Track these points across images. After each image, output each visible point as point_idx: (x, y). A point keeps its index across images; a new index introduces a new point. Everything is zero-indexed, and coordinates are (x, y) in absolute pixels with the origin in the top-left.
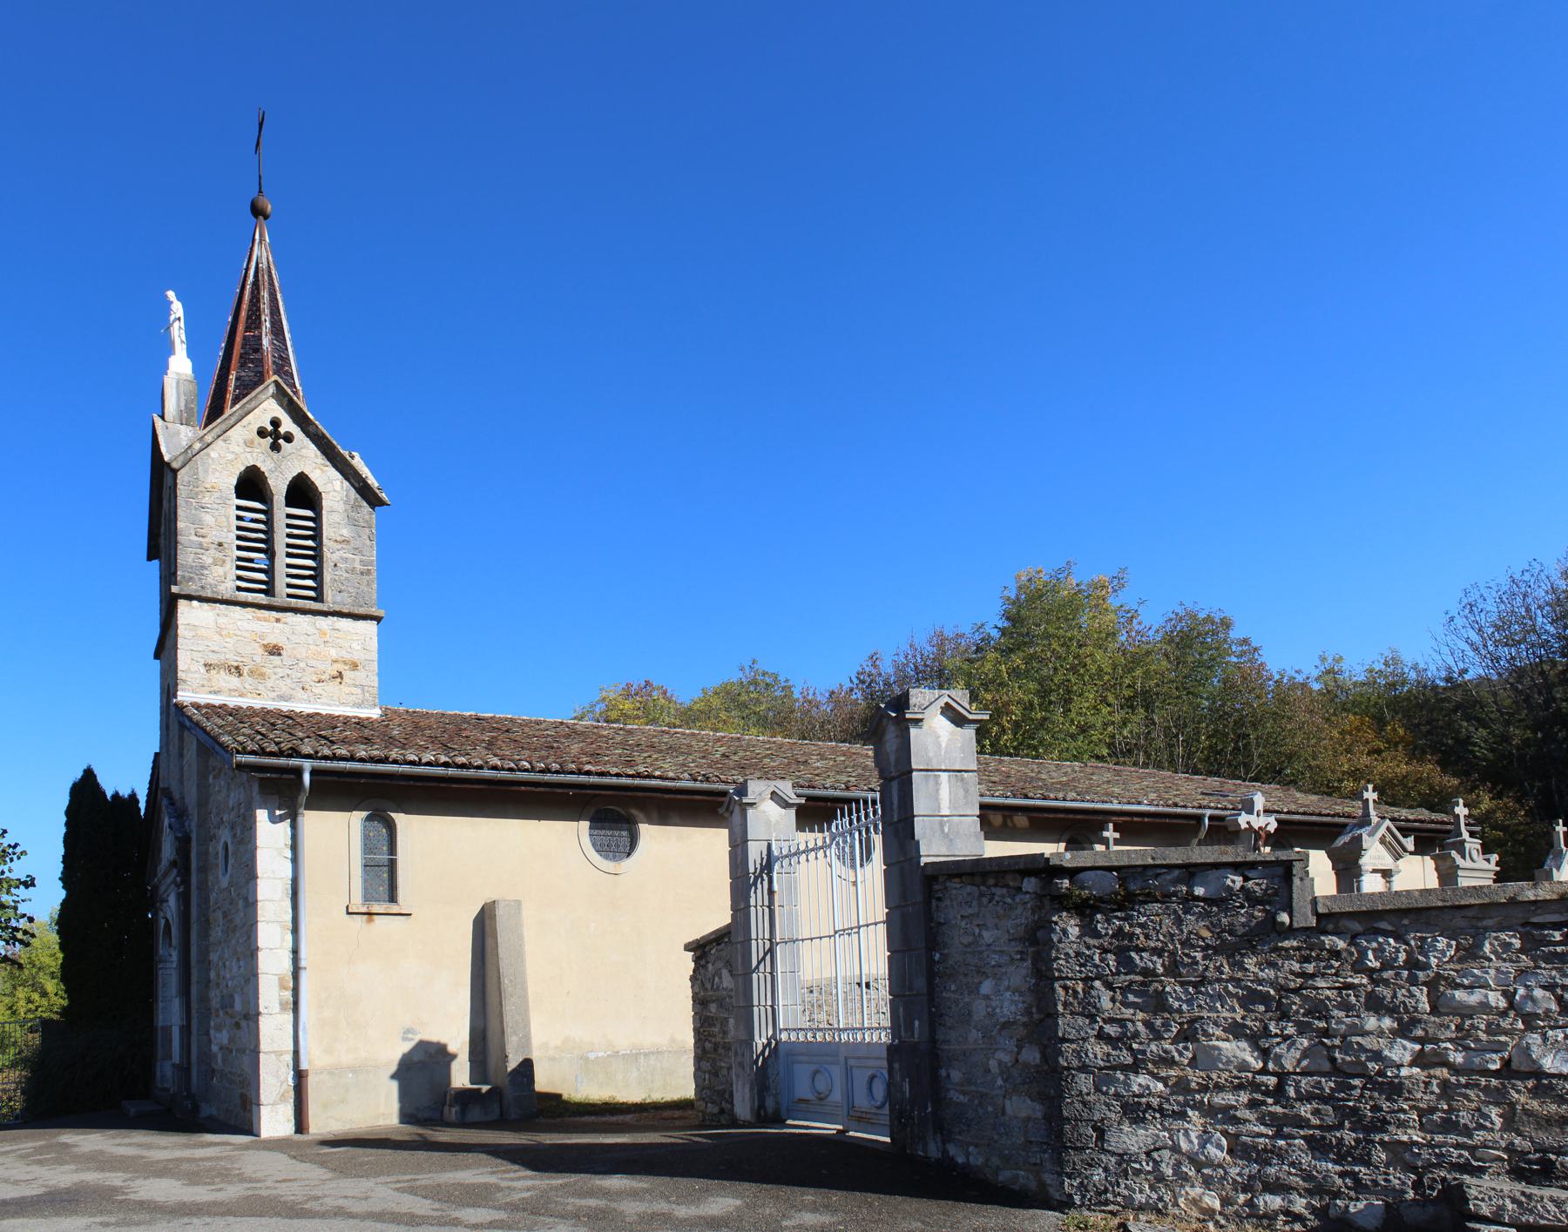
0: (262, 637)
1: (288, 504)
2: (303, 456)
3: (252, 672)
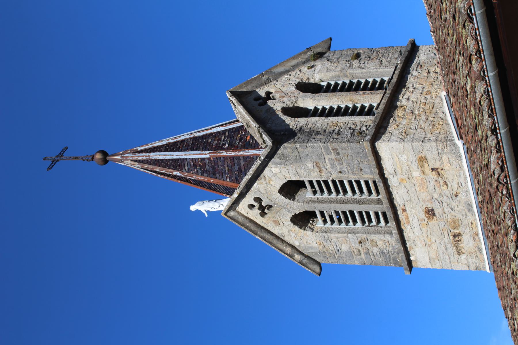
2: (266, 192)
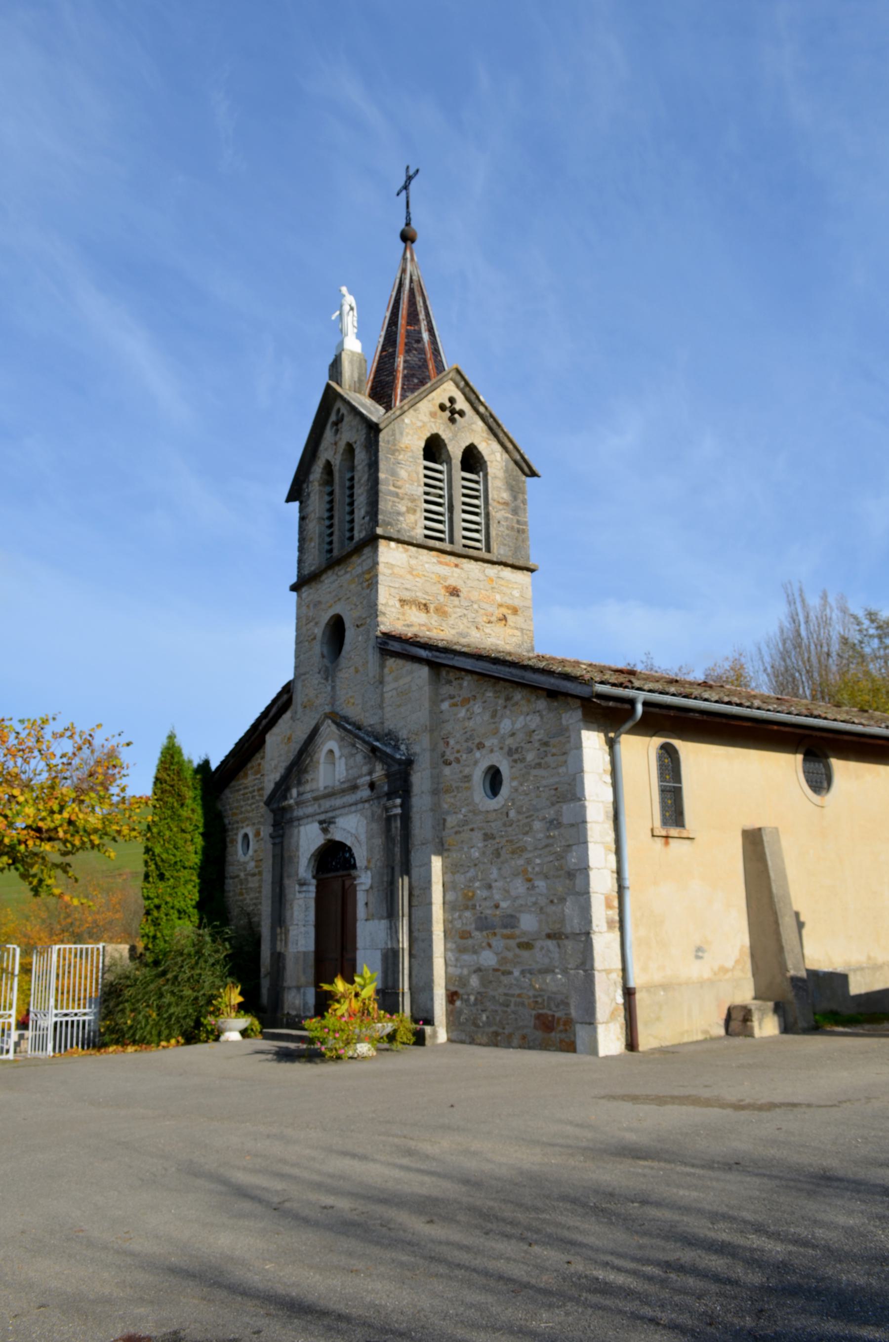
0: (445, 579)
1: (464, 469)
3: (437, 610)
